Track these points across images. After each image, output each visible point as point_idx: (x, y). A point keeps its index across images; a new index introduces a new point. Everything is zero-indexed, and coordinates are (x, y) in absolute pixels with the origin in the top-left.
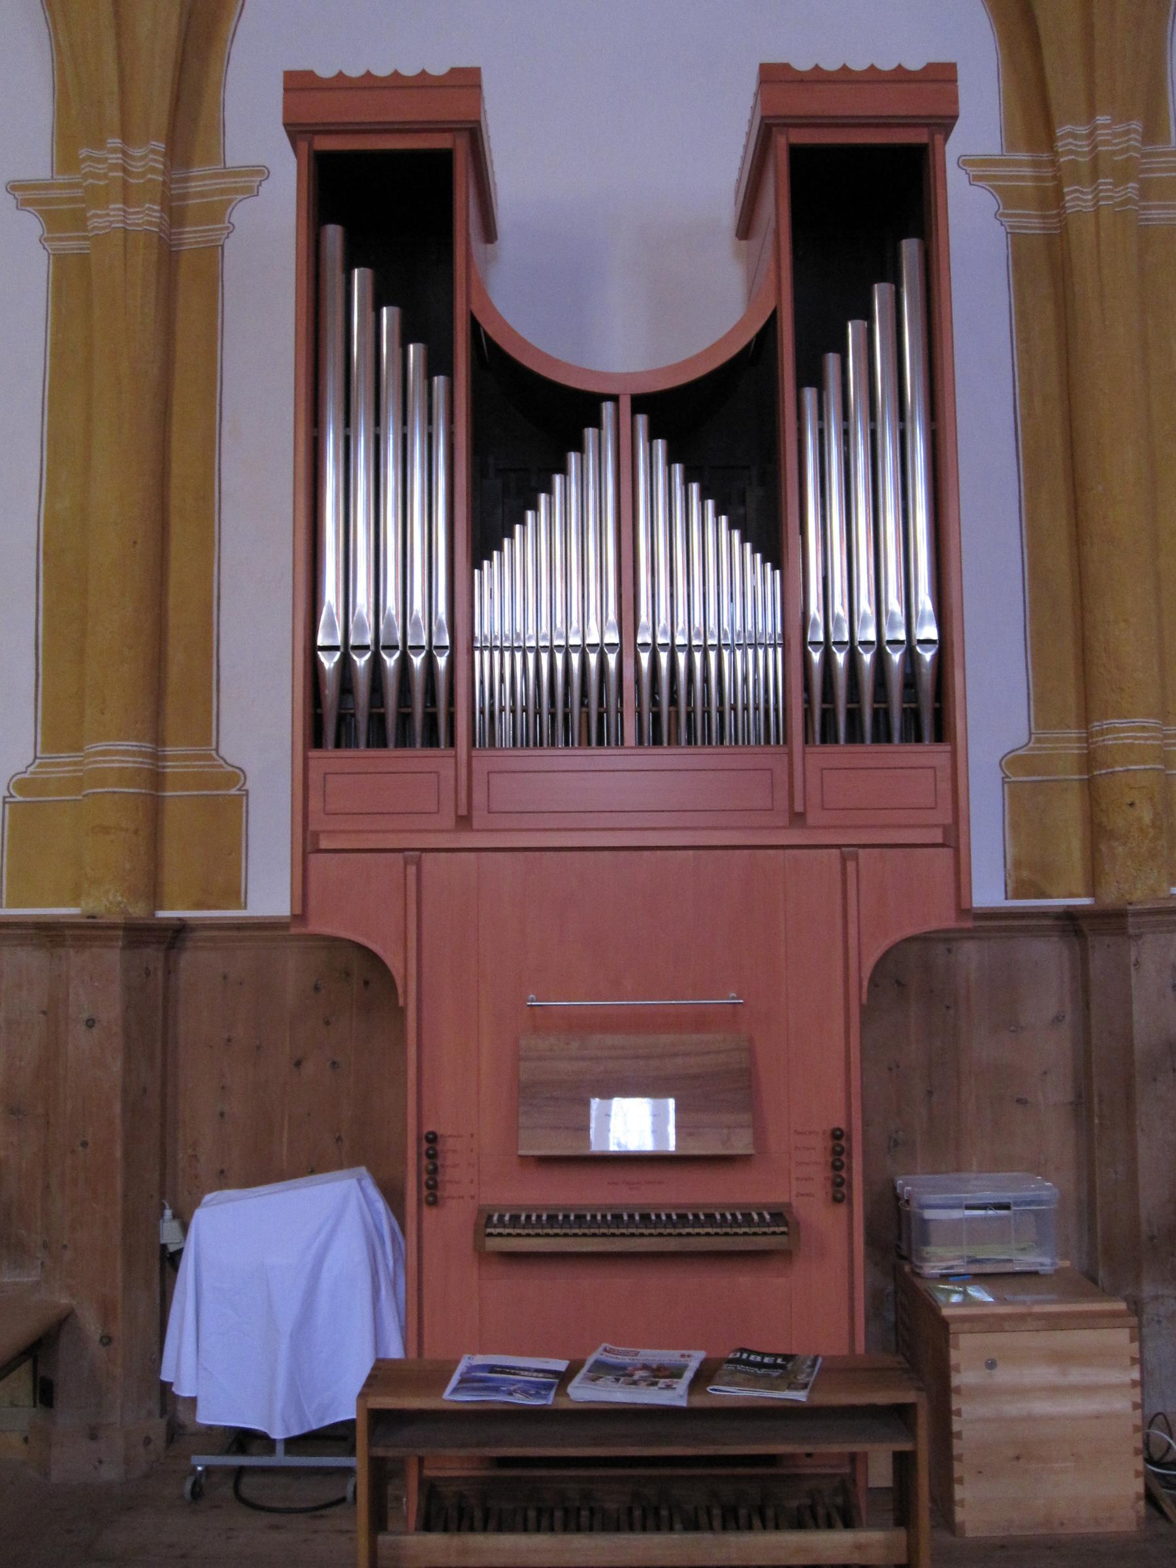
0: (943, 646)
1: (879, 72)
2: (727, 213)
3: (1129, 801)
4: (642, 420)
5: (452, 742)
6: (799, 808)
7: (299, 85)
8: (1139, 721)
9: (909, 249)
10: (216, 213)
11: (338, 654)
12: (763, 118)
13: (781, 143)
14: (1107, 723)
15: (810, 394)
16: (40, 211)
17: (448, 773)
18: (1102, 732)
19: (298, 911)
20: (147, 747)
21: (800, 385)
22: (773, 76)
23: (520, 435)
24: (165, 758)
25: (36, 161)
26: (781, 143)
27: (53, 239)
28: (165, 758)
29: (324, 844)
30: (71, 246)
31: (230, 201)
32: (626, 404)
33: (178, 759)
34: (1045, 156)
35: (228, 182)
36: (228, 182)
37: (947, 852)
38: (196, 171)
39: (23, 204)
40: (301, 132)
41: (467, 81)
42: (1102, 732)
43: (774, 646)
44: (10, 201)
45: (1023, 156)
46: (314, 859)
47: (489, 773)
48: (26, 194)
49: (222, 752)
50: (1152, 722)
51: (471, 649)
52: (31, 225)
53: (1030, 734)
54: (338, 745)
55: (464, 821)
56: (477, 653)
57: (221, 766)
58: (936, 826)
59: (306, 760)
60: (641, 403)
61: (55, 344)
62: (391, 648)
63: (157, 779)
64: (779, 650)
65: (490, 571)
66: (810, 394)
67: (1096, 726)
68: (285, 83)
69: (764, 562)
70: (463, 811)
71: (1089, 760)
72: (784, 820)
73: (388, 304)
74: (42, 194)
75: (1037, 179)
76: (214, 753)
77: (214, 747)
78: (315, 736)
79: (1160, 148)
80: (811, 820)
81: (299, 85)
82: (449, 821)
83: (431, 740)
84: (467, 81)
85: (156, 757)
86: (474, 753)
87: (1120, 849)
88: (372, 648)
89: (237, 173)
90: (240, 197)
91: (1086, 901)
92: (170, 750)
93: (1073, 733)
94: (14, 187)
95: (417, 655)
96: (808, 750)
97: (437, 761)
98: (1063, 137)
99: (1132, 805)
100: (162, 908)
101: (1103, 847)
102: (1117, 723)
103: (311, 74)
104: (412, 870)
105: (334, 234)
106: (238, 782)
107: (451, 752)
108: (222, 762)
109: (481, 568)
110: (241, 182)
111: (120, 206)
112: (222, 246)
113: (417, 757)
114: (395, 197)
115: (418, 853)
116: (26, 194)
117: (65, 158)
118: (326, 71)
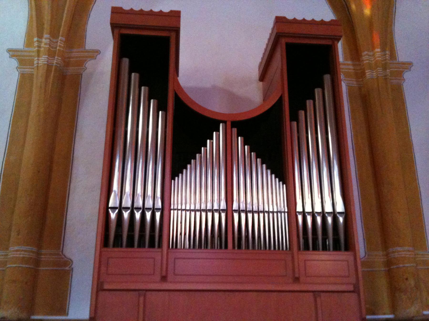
0: (347, 214)
1: (315, 21)
2: (255, 73)
3: (405, 277)
4: (235, 130)
5: (160, 246)
6: (297, 275)
7: (116, 11)
8: (406, 248)
9: (327, 78)
10: (81, 63)
11: (117, 211)
12: (277, 33)
13: (283, 41)
14: (395, 249)
15: (295, 124)
16: (18, 59)
17: (159, 258)
18: (393, 252)
19: (93, 315)
20: (35, 249)
21: (291, 120)
22: (280, 21)
23: (188, 135)
24: (41, 254)
25: (19, 43)
26: (283, 41)
27: (21, 68)
28: (41, 254)
29: (106, 287)
30: (27, 70)
31: (86, 60)
32: (229, 124)
33: (47, 254)
34: (357, 63)
35: (86, 54)
36: (86, 54)
37: (354, 295)
38: (75, 50)
39: (12, 56)
40: (116, 27)
41: (175, 15)
42: (393, 252)
43: (284, 212)
44: (8, 55)
45: (350, 62)
46: (101, 293)
47: (175, 259)
48: (13, 53)
49: (64, 252)
50: (411, 248)
51: (170, 210)
52: (14, 63)
53: (366, 253)
54: (114, 246)
55: (164, 278)
56: (172, 212)
57: (63, 258)
58: (351, 284)
59: (101, 252)
60: (234, 124)
61: (18, 99)
62: (138, 209)
63: (37, 262)
64: (286, 214)
65: (178, 180)
66: (295, 124)
67: (391, 250)
68: (112, 10)
69: (279, 181)
70: (164, 274)
71: (389, 263)
72: (291, 280)
73: (144, 85)
74: (19, 54)
75: (354, 69)
76: (61, 253)
77: (61, 250)
78: (105, 242)
79: (395, 62)
80: (302, 279)
81: (116, 11)
82: (158, 278)
83: (152, 245)
84: (175, 15)
85: (38, 254)
86: (169, 250)
87: (403, 296)
88: (131, 208)
89: (88, 51)
90: (89, 59)
91: (391, 316)
92: (44, 251)
93: (381, 253)
94: (9, 51)
95: (148, 212)
96: (299, 252)
97: (155, 253)
98: (365, 56)
99: (407, 279)
100: (33, 314)
101: (397, 295)
102: (399, 249)
103: (121, 8)
104: (142, 299)
105: (126, 61)
106: (69, 264)
107: (160, 250)
108: (63, 257)
109: (175, 180)
110: (90, 54)
111: (47, 56)
112: (82, 74)
113: (146, 252)
114: (149, 50)
115: (144, 292)
116: (13, 53)
117: (29, 42)
118: (127, 8)
